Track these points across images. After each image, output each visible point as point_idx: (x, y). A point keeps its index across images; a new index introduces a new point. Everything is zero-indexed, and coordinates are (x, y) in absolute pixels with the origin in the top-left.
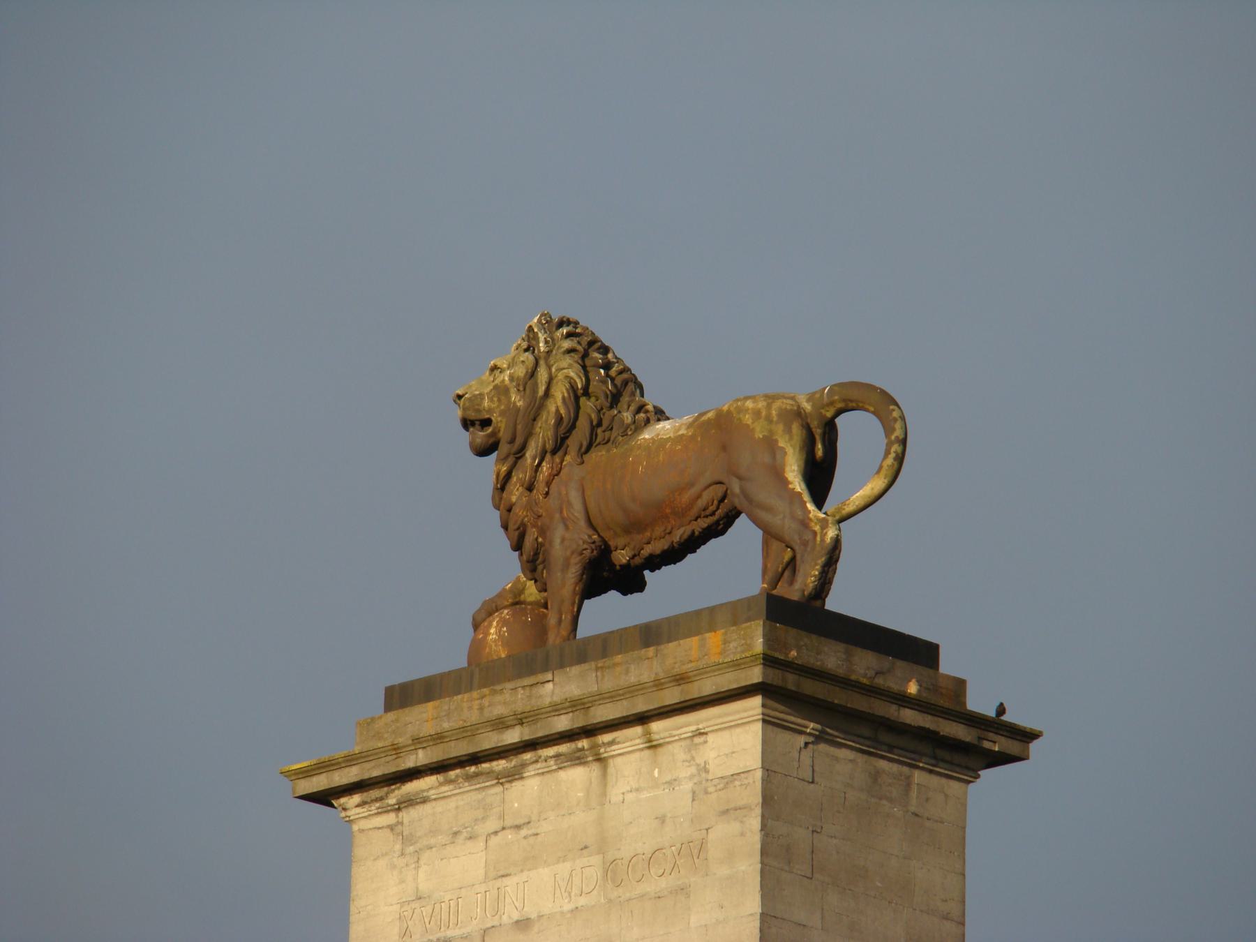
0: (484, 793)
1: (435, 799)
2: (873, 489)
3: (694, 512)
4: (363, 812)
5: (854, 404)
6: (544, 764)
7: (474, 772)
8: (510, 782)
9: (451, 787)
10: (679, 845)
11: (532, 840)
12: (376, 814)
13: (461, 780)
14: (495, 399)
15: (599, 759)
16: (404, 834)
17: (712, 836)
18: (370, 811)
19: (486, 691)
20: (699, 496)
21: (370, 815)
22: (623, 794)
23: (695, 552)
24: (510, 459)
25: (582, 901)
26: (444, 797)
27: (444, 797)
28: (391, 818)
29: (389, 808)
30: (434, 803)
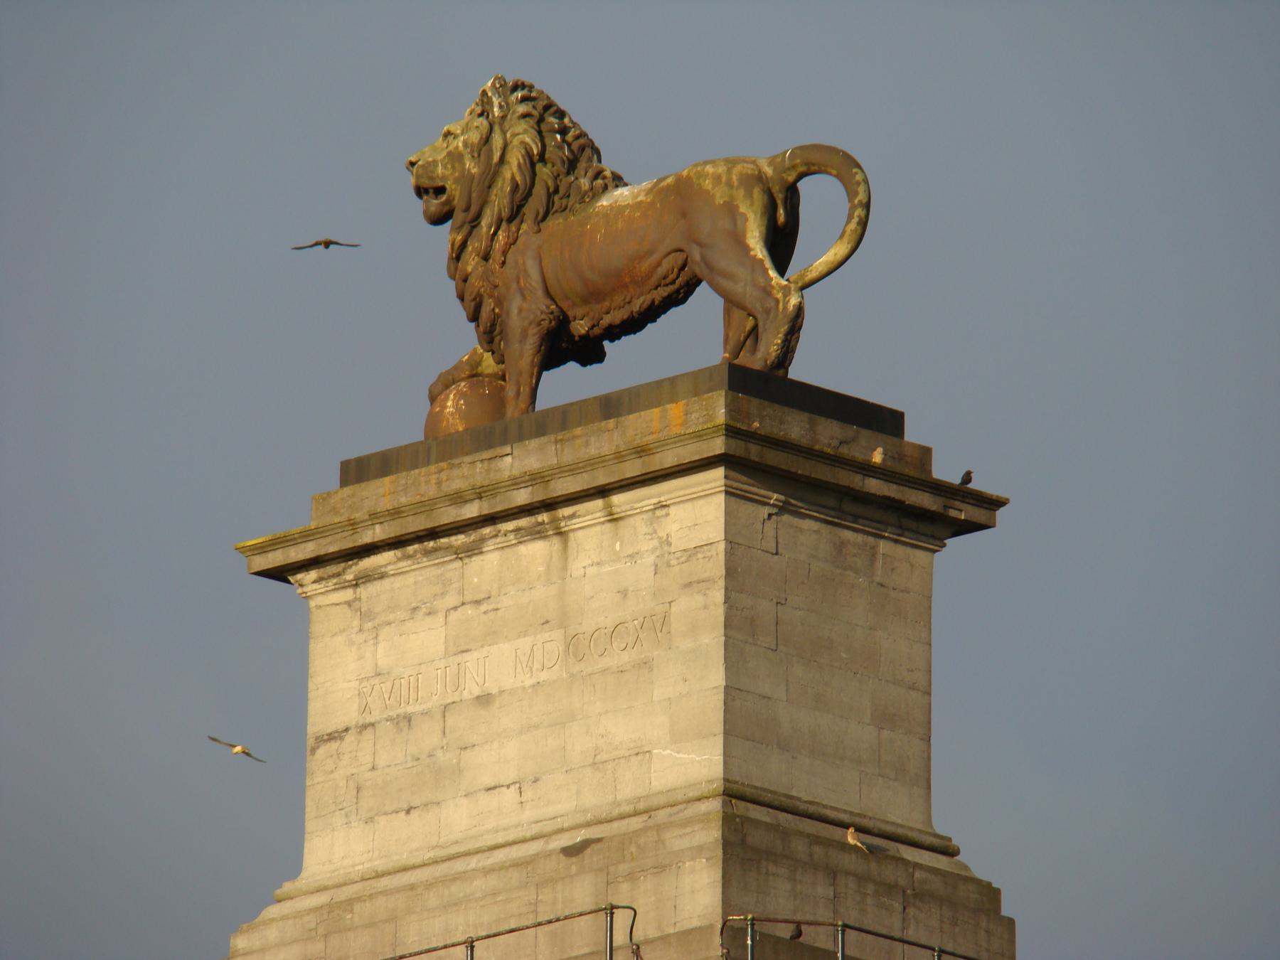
0: (443, 569)
1: (393, 575)
2: (836, 254)
3: (654, 280)
4: (320, 588)
5: (816, 168)
6: (504, 539)
7: (432, 547)
8: (470, 556)
9: (410, 562)
10: (641, 619)
11: (492, 615)
12: (333, 590)
13: (419, 555)
14: (449, 166)
15: (560, 534)
16: (362, 610)
17: (674, 608)
18: (327, 587)
19: (443, 465)
20: (659, 264)
21: (327, 591)
22: (584, 567)
23: (655, 321)
24: (465, 228)
25: (544, 676)
26: (402, 573)
27: (402, 573)
28: (348, 594)
29: (347, 584)
30: (392, 579)
